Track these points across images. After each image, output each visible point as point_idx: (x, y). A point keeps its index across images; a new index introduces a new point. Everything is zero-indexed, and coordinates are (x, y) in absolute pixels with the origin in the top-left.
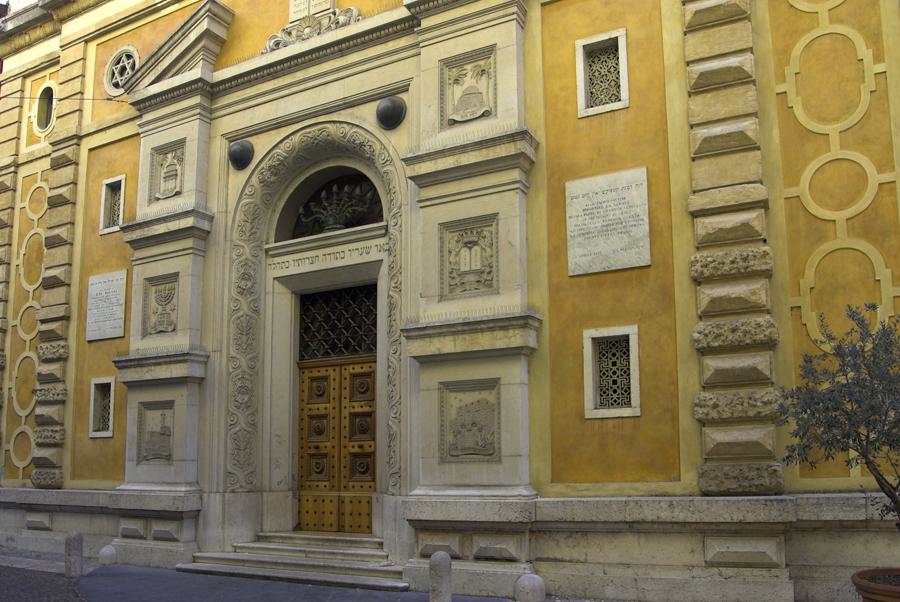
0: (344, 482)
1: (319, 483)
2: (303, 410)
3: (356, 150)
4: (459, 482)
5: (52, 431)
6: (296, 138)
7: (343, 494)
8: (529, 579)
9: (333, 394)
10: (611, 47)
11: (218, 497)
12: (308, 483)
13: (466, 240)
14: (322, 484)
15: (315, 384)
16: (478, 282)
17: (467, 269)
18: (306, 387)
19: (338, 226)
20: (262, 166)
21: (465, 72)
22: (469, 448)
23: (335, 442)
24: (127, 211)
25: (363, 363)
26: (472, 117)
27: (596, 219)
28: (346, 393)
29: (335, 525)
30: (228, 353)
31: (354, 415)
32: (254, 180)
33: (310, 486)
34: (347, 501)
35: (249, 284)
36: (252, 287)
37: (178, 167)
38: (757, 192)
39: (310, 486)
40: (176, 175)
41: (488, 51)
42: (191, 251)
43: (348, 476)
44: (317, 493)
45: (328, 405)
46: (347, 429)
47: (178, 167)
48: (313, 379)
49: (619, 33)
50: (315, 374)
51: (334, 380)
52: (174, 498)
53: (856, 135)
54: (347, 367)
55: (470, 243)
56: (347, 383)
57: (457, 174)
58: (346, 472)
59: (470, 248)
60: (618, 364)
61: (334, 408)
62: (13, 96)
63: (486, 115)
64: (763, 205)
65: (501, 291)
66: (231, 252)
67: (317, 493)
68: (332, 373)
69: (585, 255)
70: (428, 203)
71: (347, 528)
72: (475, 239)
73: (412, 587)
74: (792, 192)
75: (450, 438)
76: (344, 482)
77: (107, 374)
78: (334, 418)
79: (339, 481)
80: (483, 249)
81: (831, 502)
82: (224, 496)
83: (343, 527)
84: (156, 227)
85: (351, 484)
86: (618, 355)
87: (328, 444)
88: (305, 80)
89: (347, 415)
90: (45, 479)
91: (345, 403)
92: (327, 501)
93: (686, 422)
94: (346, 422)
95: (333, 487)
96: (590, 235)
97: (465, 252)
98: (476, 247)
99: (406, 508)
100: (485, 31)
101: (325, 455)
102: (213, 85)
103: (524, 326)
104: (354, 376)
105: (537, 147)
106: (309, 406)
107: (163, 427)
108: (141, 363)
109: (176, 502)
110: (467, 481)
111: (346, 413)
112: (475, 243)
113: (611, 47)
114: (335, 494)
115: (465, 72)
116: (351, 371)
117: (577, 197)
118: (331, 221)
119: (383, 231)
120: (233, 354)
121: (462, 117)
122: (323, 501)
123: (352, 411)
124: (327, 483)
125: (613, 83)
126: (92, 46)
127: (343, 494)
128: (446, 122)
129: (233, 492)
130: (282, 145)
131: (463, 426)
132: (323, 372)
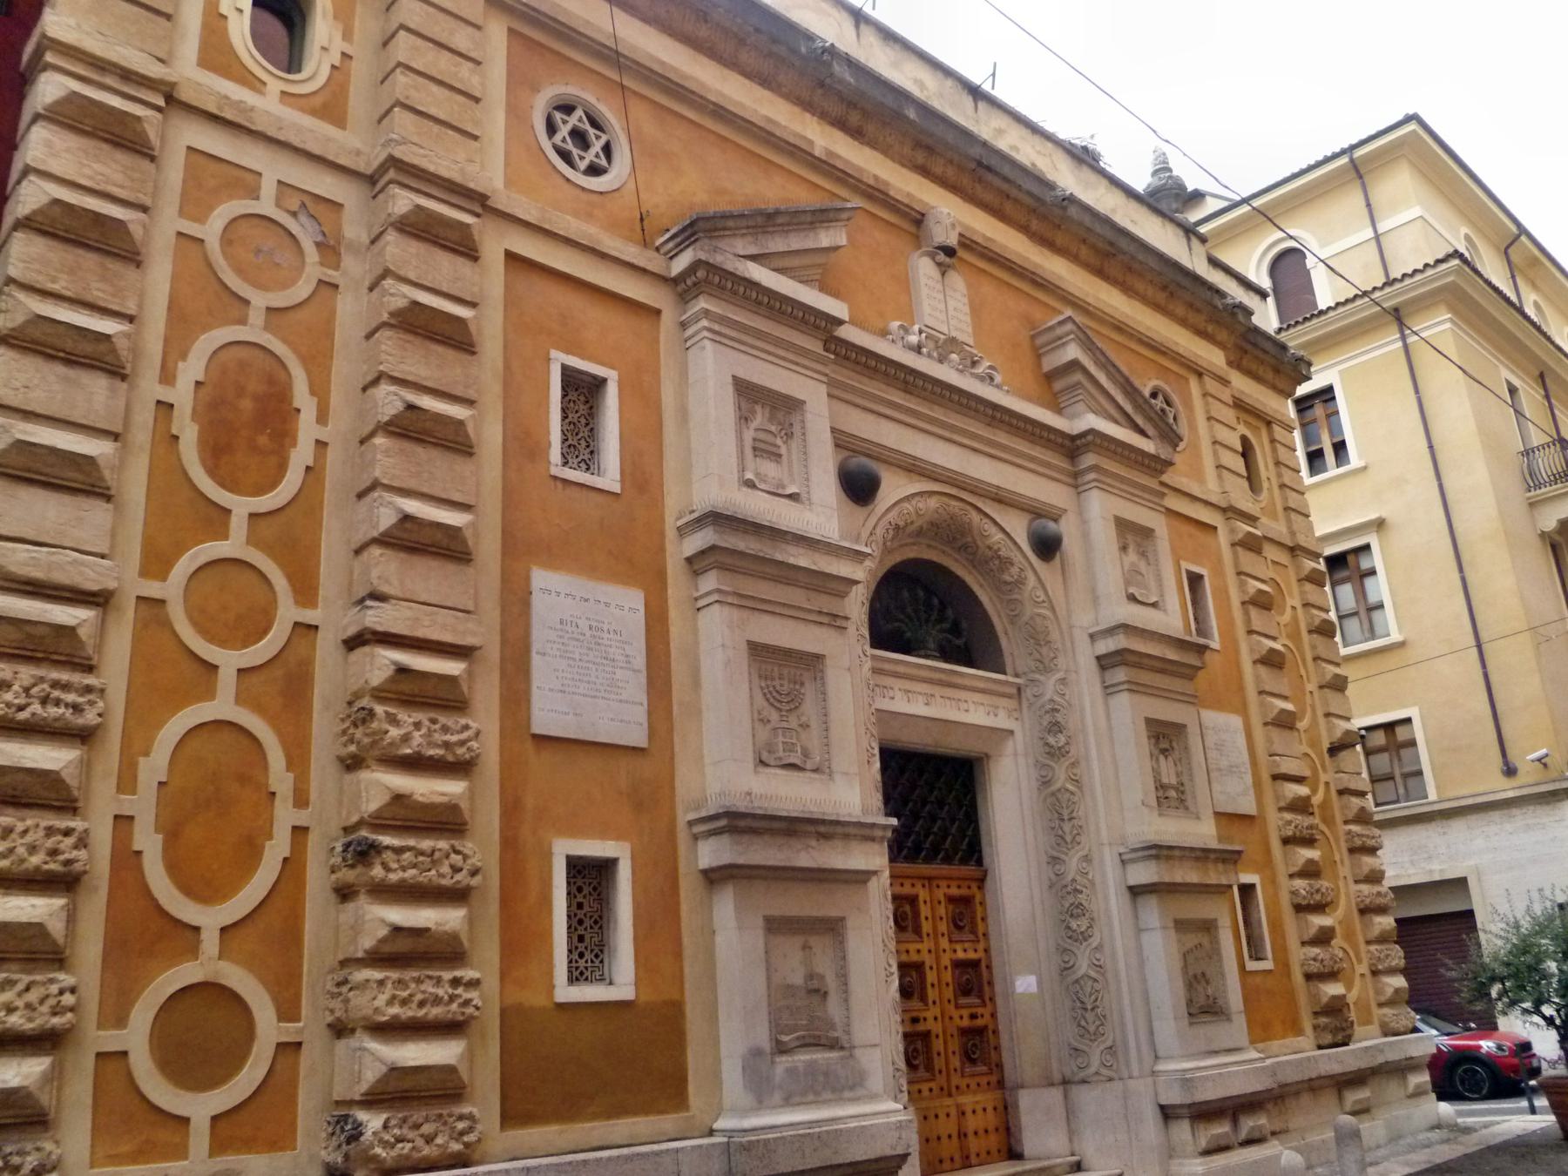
0: (956, 1080)
3: (992, 564)
5: (456, 982)
6: (933, 503)
8: (1289, 1157)
14: (984, 1080)
29: (957, 1158)
31: (958, 964)
36: (1067, 743)
38: (91, 576)
42: (1126, 686)
46: (951, 988)
47: (779, 442)
53: (216, 520)
57: (768, 570)
58: (956, 1062)
60: (586, 908)
64: (98, 599)
71: (974, 1160)
74: (153, 589)
76: (956, 1080)
77: (604, 833)
83: (967, 1157)
84: (792, 549)
86: (586, 891)
88: (952, 428)
89: (948, 963)
90: (429, 1140)
91: (944, 943)
93: (1298, 977)
102: (1073, 438)
104: (951, 900)
107: (811, 976)
111: (946, 960)
114: (948, 1101)
121: (1142, 594)
123: (954, 957)
124: (932, 1085)
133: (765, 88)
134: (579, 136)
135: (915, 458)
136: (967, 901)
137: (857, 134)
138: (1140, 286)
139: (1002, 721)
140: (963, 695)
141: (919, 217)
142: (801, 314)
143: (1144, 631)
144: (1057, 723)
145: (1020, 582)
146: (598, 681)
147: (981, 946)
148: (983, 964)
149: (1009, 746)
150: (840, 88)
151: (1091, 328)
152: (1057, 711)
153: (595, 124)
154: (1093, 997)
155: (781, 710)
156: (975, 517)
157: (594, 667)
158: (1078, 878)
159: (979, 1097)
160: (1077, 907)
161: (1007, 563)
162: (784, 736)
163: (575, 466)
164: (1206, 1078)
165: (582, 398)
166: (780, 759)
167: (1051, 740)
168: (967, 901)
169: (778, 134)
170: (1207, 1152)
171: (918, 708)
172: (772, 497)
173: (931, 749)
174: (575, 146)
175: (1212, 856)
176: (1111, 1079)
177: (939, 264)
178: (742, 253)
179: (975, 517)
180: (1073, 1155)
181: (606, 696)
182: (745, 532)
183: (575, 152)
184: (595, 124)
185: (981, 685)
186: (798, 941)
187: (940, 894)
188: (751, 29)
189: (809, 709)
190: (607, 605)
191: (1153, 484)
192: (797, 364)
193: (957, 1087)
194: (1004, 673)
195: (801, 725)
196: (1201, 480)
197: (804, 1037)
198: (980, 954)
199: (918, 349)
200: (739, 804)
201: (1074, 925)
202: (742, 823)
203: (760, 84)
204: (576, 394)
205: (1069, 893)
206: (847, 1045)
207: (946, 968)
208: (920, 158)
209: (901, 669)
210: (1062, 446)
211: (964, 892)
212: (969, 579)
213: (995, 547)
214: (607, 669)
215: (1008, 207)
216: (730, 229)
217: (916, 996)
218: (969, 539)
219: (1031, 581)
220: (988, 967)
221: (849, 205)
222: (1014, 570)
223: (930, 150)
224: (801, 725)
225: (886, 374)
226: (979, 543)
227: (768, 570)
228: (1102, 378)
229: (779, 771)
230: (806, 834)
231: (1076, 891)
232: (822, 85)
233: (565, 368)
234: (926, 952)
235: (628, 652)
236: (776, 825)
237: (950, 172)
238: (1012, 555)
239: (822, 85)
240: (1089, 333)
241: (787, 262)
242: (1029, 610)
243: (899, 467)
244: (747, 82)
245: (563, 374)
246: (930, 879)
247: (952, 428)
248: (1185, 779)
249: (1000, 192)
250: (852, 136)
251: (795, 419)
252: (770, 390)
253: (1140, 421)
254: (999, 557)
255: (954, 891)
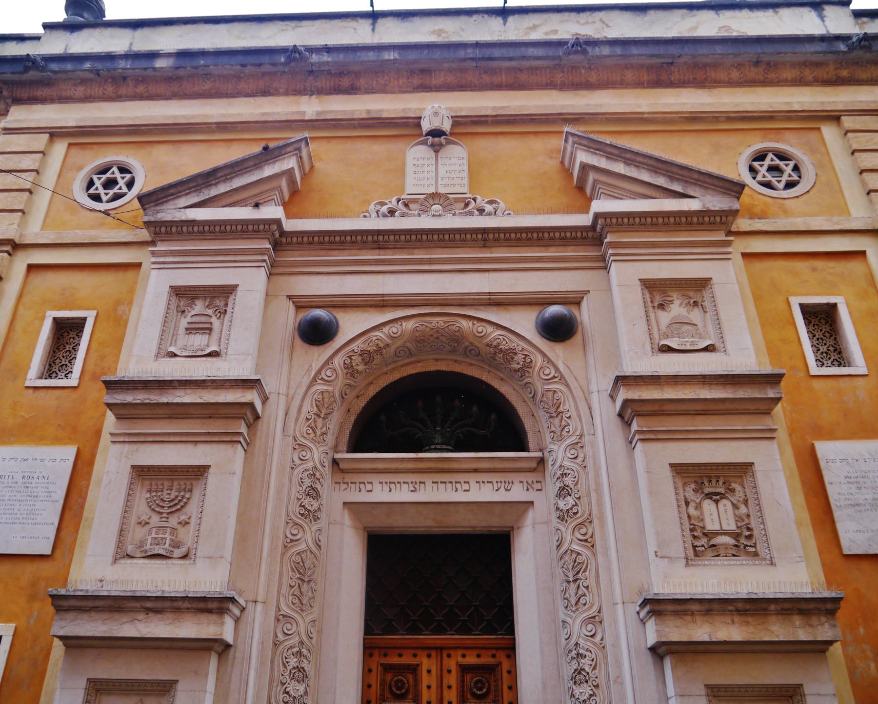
6: (409, 325)
10: (77, 325)
13: (707, 490)
15: (388, 677)
16: (736, 546)
18: (374, 680)
19: (449, 447)
24: (90, 367)
25: (467, 648)
26: (692, 348)
27: (863, 490)
30: (279, 609)
32: (338, 361)
35: (316, 505)
37: (214, 320)
40: (210, 329)
41: (226, 291)
48: (387, 668)
49: (795, 302)
50: (395, 660)
51: (429, 671)
54: (452, 653)
55: (716, 494)
56: (452, 679)
59: (717, 502)
62: (23, 175)
63: (709, 349)
65: (776, 561)
69: (860, 531)
80: (734, 505)
88: (430, 261)
96: (862, 508)
97: (708, 506)
98: (724, 501)
103: (831, 613)
104: (464, 669)
108: (175, 604)
112: (723, 496)
113: (77, 325)
116: (460, 659)
117: (833, 461)
118: (438, 439)
120: (285, 610)
125: (831, 348)
126: (60, 148)
128: (656, 348)
130: (386, 329)
132: (407, 660)
133: (266, 96)
134: (110, 184)
136: (491, 670)
137: (352, 90)
138: (722, 75)
139: (517, 493)
141: (416, 121)
143: (676, 377)
145: (528, 365)
146: (19, 513)
150: (327, 68)
151: (592, 132)
153: (104, 171)
156: (465, 324)
157: (18, 503)
160: (579, 673)
161: (510, 354)
163: (63, 377)
165: (823, 321)
166: (146, 551)
167: (561, 504)
168: (491, 670)
169: (270, 119)
171: (403, 494)
172: (189, 359)
173: (436, 531)
174: (112, 189)
175: (772, 607)
177: (432, 145)
178: (182, 206)
179: (465, 324)
181: (24, 521)
182: (136, 389)
183: (116, 190)
184: (104, 171)
185: (410, 465)
187: (451, 664)
188: (239, 67)
190: (42, 460)
191: (721, 236)
192: (235, 261)
194: (528, 451)
196: (844, 211)
200: (166, 589)
201: (577, 691)
202: (65, 603)
203: (263, 96)
204: (817, 320)
205: (573, 658)
208: (416, 81)
209: (380, 466)
211: (486, 660)
212: (485, 377)
213: (495, 343)
214: (29, 503)
215: (523, 77)
216: (172, 194)
218: (467, 344)
222: (519, 357)
223: (424, 72)
224: (180, 523)
226: (477, 344)
227: (161, 412)
229: (141, 561)
230: (133, 610)
231: (579, 655)
232: (311, 72)
233: (84, 319)
235: (50, 490)
236: (97, 603)
237: (451, 79)
238: (512, 345)
239: (311, 72)
240: (592, 136)
241: (236, 198)
242: (540, 387)
243: (371, 306)
244: (251, 99)
245: (802, 312)
246: (440, 649)
247: (430, 261)
249: (509, 70)
250: (349, 93)
251: (706, 294)
252: (204, 287)
253: (677, 187)
254: (501, 350)
255: (471, 659)
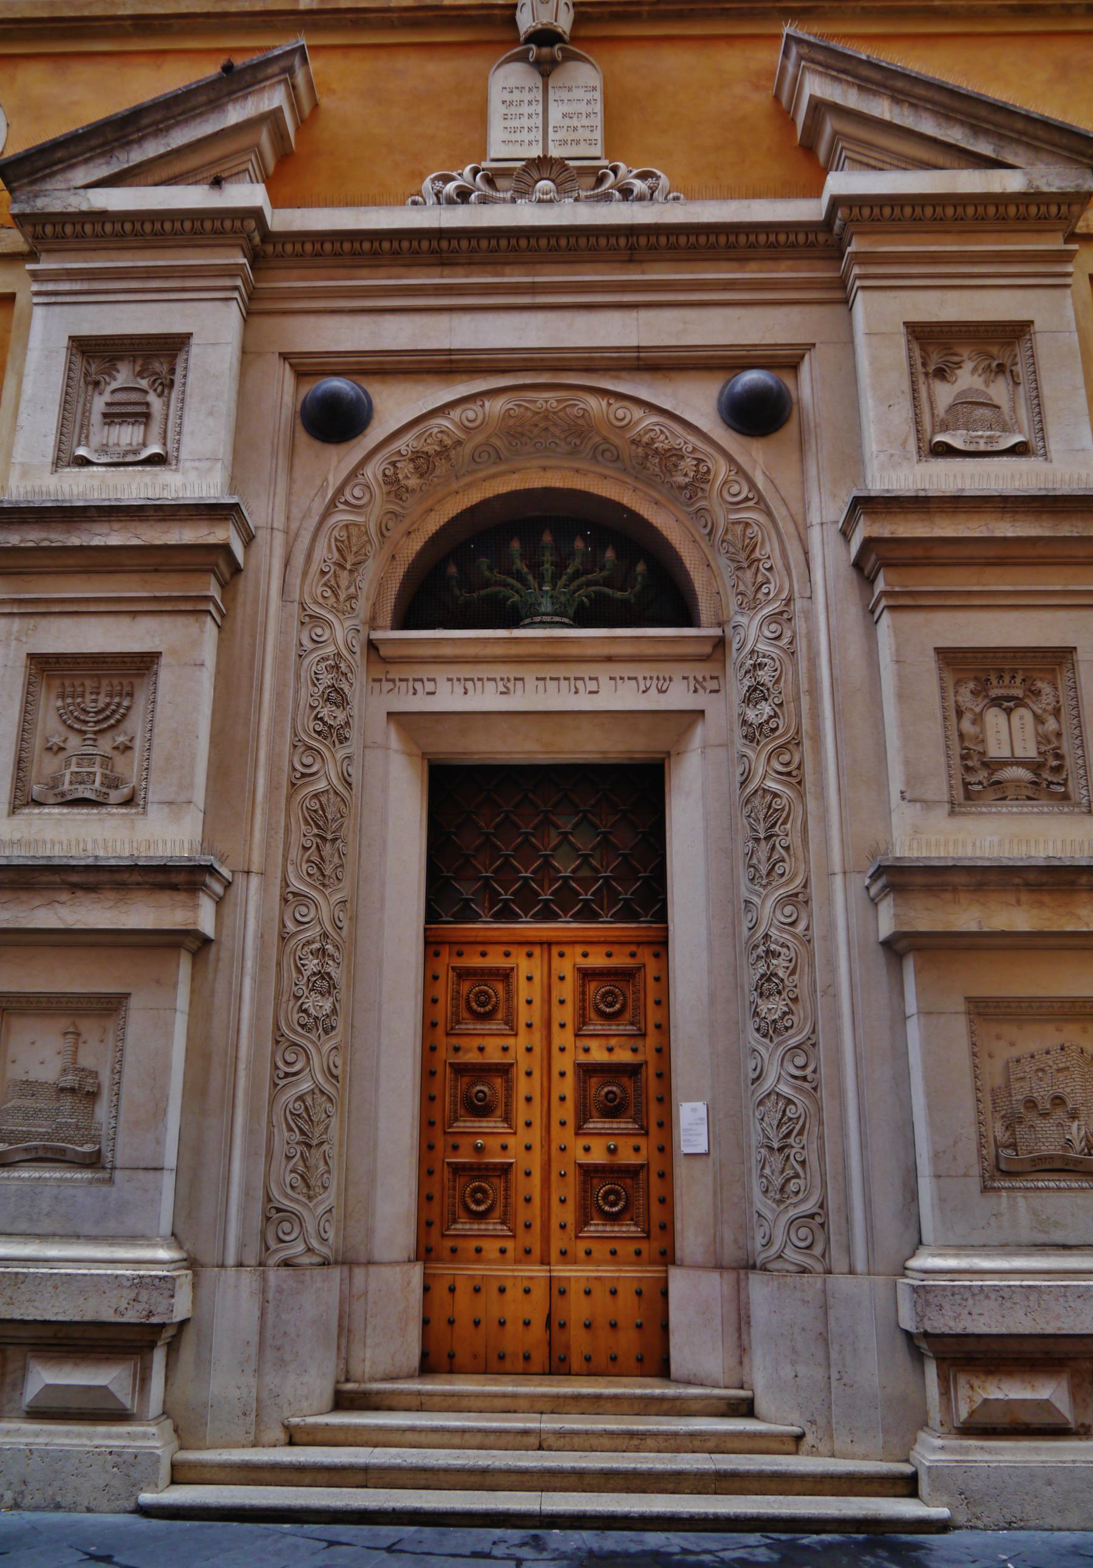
0: (557, 1243)
1: (486, 1244)
2: (433, 1049)
4: (1041, 1238)
6: (497, 406)
7: (562, 1271)
9: (523, 1014)
11: (248, 1279)
12: (449, 1243)
13: (995, 692)
14: (631, 1247)
15: (465, 987)
17: (1006, 753)
20: (400, 444)
21: (956, 359)
22: (1051, 1157)
23: (535, 1136)
28: (566, 1014)
31: (586, 1071)
33: (454, 1250)
34: (575, 1292)
35: (341, 717)
37: (152, 398)
39: (454, 1250)
43: (571, 1227)
44: (478, 1270)
45: (510, 1042)
47: (152, 398)
48: (463, 974)
52: (140, 1283)
54: (566, 949)
56: (567, 990)
59: (1009, 712)
61: (529, 1050)
63: (1019, 450)
66: (299, 632)
67: (478, 1270)
68: (524, 965)
70: (42, 609)
72: (1018, 692)
73: (961, 1519)
75: (998, 1130)
78: (529, 1074)
79: (546, 1239)
81: (1033, 1297)
82: (264, 1279)
85: (582, 1246)
87: (511, 1141)
91: (564, 1038)
92: (514, 1293)
94: (567, 1087)
95: (528, 1252)
98: (1022, 711)
99: (928, 1304)
100: (1006, 293)
101: (505, 1169)
104: (586, 975)
105: (249, 539)
106: (455, 1041)
108: (117, 877)
109: (144, 1296)
110: (1058, 1237)
111: (564, 1063)
112: (1020, 702)
114: (538, 1272)
115: (956, 359)
118: (546, 606)
119: (707, 649)
120: (297, 885)
122: (502, 1290)
123: (583, 1058)
124: (509, 1245)
127: (562, 1271)
128: (926, 447)
129: (286, 1263)
130: (455, 414)
131: (1031, 1103)
135: (450, 352)
140: (425, 671)
141: (508, 12)
142: (1054, 210)
144: (339, 691)
147: (652, 1041)
148: (651, 1071)
149: (698, 734)
151: (833, 36)
152: (761, 666)
154: (784, 1129)
155: (85, 732)
158: (773, 932)
159: (607, 1272)
160: (769, 980)
162: (79, 765)
164: (954, 1291)
166: (63, 794)
167: (751, 715)
170: (968, 1430)
176: (804, 1271)
180: (742, 1388)
186: (63, 1023)
187: (566, 967)
189: (136, 724)
193: (563, 1253)
195: (116, 748)
197: (36, 1148)
198: (647, 1053)
199: (463, 195)
206: (108, 1166)
207: (562, 1074)
210: (809, 245)
211: (621, 960)
213: (645, 439)
217: (498, 1112)
219: (721, 470)
220: (659, 1076)
221: (277, 52)
224: (116, 748)
225: (672, 247)
228: (881, 108)
234: (521, 1050)
238: (676, 443)
240: (834, 44)
248: (1067, 747)
255: (597, 960)
